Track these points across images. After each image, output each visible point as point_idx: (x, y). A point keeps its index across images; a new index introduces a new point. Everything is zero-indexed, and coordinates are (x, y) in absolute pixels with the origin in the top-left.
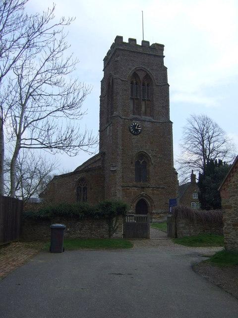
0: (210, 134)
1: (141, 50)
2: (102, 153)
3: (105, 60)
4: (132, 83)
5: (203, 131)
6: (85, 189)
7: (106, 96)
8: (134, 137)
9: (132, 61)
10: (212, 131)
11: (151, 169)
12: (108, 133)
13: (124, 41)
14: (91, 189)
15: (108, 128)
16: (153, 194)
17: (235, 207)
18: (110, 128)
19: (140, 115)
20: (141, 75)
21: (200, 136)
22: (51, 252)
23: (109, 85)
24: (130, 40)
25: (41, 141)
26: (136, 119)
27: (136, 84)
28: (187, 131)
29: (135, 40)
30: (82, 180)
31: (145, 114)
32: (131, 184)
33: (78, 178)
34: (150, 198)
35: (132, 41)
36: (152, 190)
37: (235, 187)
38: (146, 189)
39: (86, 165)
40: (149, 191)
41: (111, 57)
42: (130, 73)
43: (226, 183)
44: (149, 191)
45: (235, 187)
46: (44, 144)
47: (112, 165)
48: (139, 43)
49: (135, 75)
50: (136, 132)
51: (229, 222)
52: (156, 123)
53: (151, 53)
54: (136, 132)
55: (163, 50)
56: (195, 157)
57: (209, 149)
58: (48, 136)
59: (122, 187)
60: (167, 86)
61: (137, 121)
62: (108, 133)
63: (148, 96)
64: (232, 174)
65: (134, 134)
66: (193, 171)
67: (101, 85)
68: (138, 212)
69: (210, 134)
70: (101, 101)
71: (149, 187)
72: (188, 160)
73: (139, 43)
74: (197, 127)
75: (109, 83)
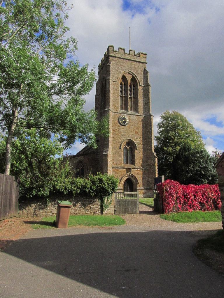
7: (100, 95)
8: (123, 127)
13: (221, 228)
20: (129, 78)
23: (102, 86)
27: (124, 85)
30: (80, 162)
32: (120, 165)
39: (84, 151)
50: (124, 124)
53: (136, 60)
59: (113, 168)
60: (112, 294)
68: (125, 189)
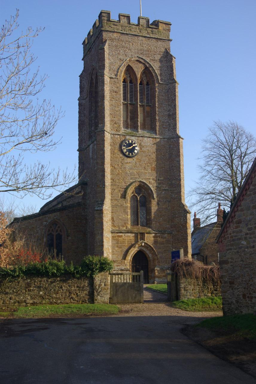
0: (243, 150)
2: (82, 184)
5: (232, 146)
8: (129, 160)
10: (246, 146)
12: (91, 154)
15: (91, 146)
17: (231, 262)
18: (93, 147)
20: (139, 70)
21: (228, 153)
28: (208, 146)
30: (54, 223)
33: (49, 221)
37: (232, 239)
39: (59, 200)
41: (94, 42)
43: (223, 235)
45: (232, 239)
46: (11, 186)
47: (97, 202)
49: (129, 70)
51: (226, 279)
56: (221, 186)
57: (242, 173)
58: (14, 174)
62: (91, 154)
63: (147, 99)
64: (228, 225)
65: (128, 157)
66: (219, 205)
69: (243, 150)
72: (210, 188)
74: (224, 140)
75: (92, 79)
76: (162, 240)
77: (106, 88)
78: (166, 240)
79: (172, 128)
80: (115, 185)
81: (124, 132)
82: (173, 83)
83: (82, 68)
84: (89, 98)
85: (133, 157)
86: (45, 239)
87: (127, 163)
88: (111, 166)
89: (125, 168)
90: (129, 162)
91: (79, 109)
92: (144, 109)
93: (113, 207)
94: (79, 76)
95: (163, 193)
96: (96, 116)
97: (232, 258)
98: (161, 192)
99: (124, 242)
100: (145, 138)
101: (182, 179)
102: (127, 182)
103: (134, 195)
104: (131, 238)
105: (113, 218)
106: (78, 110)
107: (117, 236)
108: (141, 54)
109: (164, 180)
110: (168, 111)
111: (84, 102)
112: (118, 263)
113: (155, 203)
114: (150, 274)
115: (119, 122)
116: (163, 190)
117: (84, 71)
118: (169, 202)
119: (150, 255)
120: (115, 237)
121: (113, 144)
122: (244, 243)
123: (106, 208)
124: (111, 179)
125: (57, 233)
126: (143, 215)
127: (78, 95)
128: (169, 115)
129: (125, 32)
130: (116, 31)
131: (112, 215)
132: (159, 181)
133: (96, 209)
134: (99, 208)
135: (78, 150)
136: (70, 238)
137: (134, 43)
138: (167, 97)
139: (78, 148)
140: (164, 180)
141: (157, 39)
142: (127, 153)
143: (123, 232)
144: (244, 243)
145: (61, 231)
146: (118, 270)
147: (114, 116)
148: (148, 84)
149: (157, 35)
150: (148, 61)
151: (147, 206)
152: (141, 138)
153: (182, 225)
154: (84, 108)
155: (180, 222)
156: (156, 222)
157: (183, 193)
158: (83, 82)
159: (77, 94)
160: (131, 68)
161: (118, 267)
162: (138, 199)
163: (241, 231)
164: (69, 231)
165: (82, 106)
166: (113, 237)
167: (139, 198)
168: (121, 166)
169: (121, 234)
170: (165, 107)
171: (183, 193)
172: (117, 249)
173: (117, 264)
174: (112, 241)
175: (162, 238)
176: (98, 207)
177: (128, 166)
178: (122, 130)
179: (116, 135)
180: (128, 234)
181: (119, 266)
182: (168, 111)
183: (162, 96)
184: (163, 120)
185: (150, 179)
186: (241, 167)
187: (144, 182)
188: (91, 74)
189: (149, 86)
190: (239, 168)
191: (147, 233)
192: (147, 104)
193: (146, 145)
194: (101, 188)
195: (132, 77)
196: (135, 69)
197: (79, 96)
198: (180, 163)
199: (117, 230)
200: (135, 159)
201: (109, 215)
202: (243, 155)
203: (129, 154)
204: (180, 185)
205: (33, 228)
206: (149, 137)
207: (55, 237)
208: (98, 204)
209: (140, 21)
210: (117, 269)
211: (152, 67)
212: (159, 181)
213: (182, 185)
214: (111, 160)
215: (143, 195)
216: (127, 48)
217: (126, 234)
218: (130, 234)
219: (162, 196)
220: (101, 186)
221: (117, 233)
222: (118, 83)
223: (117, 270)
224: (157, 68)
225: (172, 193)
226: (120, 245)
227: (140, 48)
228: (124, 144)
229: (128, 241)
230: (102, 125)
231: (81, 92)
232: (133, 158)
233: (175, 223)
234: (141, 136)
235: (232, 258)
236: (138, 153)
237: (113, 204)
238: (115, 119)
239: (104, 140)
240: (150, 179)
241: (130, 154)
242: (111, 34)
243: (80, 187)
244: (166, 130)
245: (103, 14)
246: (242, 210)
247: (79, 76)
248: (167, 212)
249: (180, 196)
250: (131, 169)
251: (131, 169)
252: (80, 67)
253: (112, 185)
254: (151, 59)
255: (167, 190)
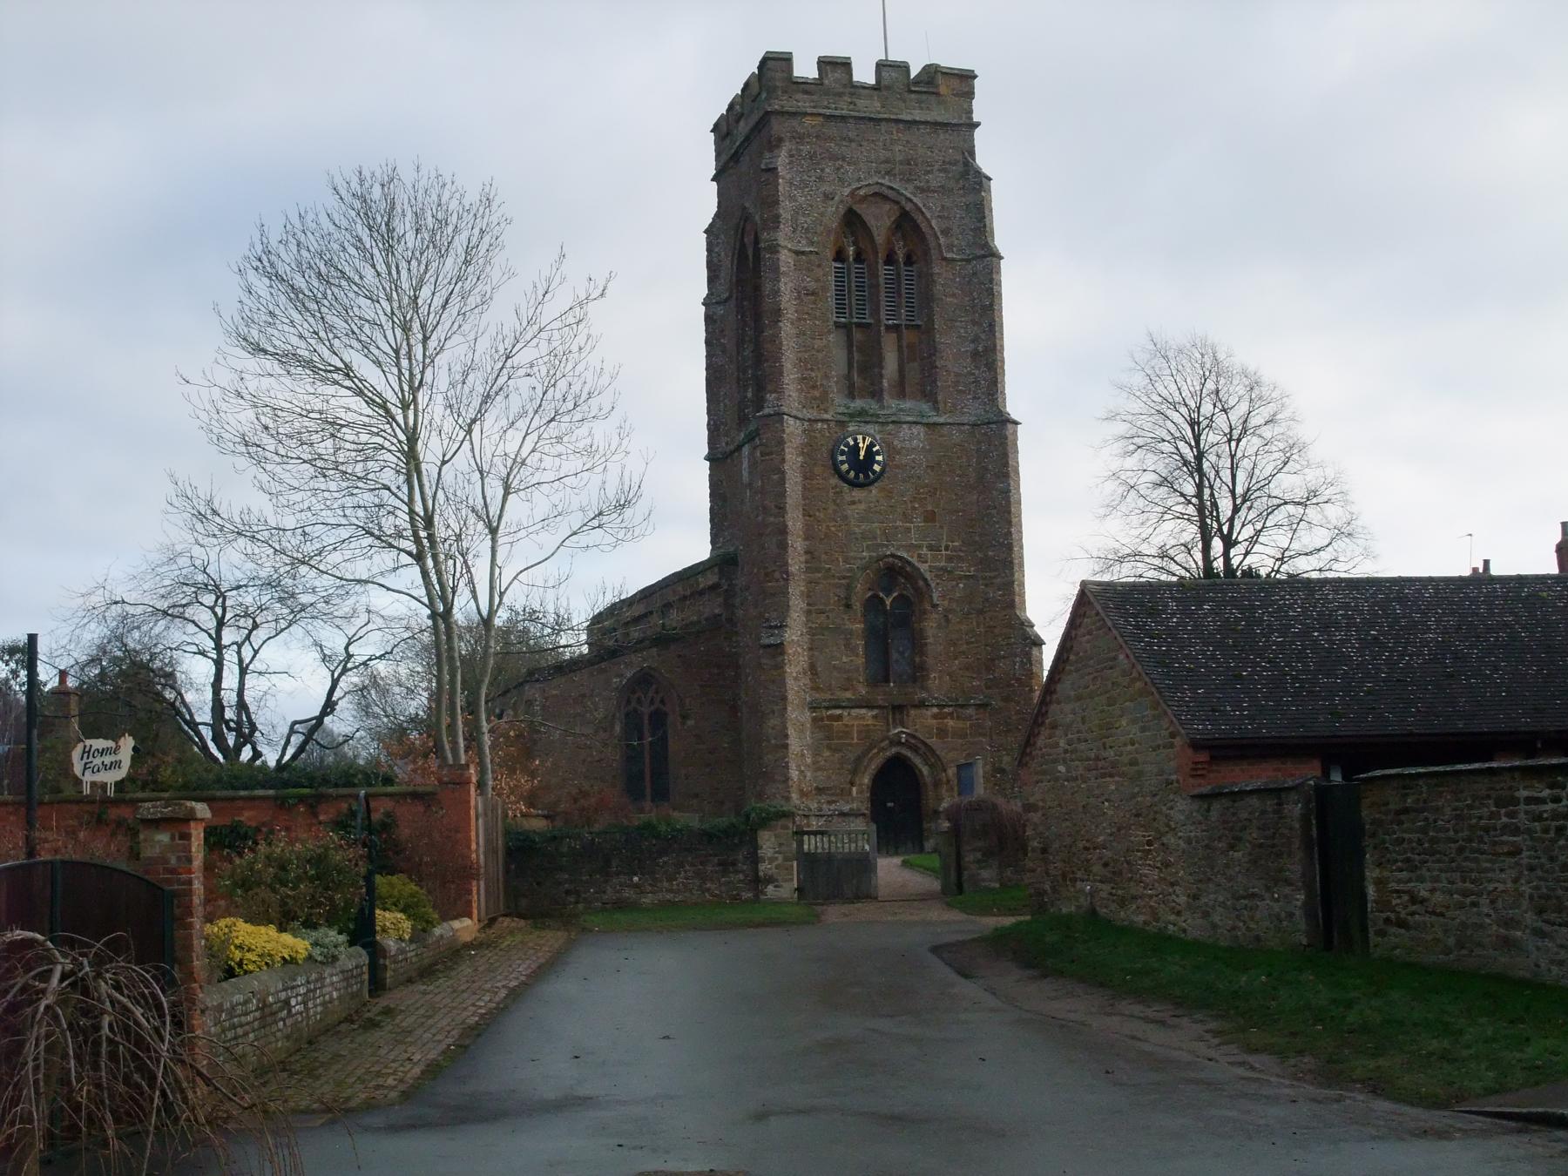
1: (871, 106)
2: (722, 562)
3: (722, 130)
4: (840, 256)
6: (658, 719)
8: (858, 494)
9: (833, 158)
11: (931, 627)
12: (745, 474)
14: (685, 717)
15: (746, 450)
16: (942, 733)
18: (751, 454)
19: (877, 394)
20: (880, 221)
22: (509, 853)
23: (741, 255)
24: (825, 64)
25: (462, 434)
26: (861, 416)
29: (845, 65)
30: (644, 680)
31: (901, 391)
32: (848, 695)
34: (928, 753)
35: (834, 67)
36: (935, 716)
38: (913, 712)
40: (923, 722)
42: (832, 215)
43: (1028, 750)
44: (923, 722)
48: (864, 74)
49: (852, 221)
52: (945, 430)
53: (918, 115)
54: (861, 471)
55: (970, 94)
59: (813, 708)
61: (870, 428)
62: (745, 474)
65: (854, 484)
67: (709, 250)
70: (709, 319)
71: (922, 705)
73: (864, 74)
75: (743, 245)
76: (960, 724)
77: (786, 284)
78: (971, 726)
79: (983, 393)
80: (818, 570)
81: (841, 410)
82: (984, 256)
83: (712, 207)
84: (737, 299)
85: (872, 483)
86: (618, 728)
87: (853, 503)
88: (804, 515)
89: (845, 518)
90: (857, 499)
91: (707, 331)
92: (899, 339)
93: (812, 632)
94: (705, 232)
95: (961, 585)
96: (759, 358)
97: (1043, 800)
98: (954, 583)
99: (847, 734)
100: (904, 426)
101: (1015, 544)
102: (855, 558)
103: (875, 596)
104: (869, 722)
105: (812, 667)
106: (703, 335)
107: (827, 716)
108: (888, 173)
109: (963, 549)
110: (973, 341)
111: (720, 310)
112: (833, 795)
113: (936, 616)
114: (926, 826)
115: (825, 382)
116: (960, 578)
117: (717, 215)
118: (981, 612)
119: (925, 770)
120: (822, 719)
121: (808, 450)
122: (1062, 768)
123: (793, 637)
124: (806, 553)
125: (652, 708)
126: (902, 653)
127: (703, 291)
128: (975, 355)
129: (837, 113)
130: (809, 110)
131: (811, 657)
132: (949, 553)
133: (766, 641)
134: (772, 641)
135: (707, 458)
136: (690, 723)
137: (865, 143)
138: (967, 299)
139: (706, 451)
140: (963, 549)
141: (936, 124)
142: (852, 474)
143: (844, 704)
144: (1062, 768)
145: (662, 701)
146: (831, 815)
147: (809, 366)
148: (909, 261)
149: (932, 113)
150: (909, 195)
151: (916, 625)
152: (891, 427)
153: (1018, 680)
154: (723, 331)
155: (1012, 672)
156: (940, 671)
157: (1019, 585)
158: (716, 250)
159: (697, 286)
160: (859, 216)
161: (832, 808)
162: (886, 605)
163: (1057, 745)
164: (687, 701)
165: (715, 321)
166: (814, 720)
167: (888, 602)
168: (835, 512)
169: (838, 712)
170: (962, 331)
171: (1019, 585)
172: (827, 754)
173: (829, 799)
174: (812, 733)
175: (958, 718)
176: (768, 637)
177: (852, 511)
178: (839, 403)
179: (817, 421)
180: (857, 710)
181: (834, 802)
182: (973, 341)
183: (954, 295)
184: (956, 370)
185: (920, 547)
186: (1232, 472)
187: (903, 558)
188: (740, 231)
189: (915, 266)
190: (1226, 475)
191: (915, 706)
192: (908, 323)
193: (908, 446)
194: (777, 581)
195: (861, 245)
196: (872, 222)
197: (705, 292)
198: (1009, 497)
199: (825, 700)
200: (874, 490)
201: (801, 658)
202: (1236, 434)
203: (857, 476)
204: (1011, 562)
205: (584, 696)
206: (916, 423)
207: (646, 718)
208: (771, 627)
209: (883, 74)
210: (829, 813)
211: (923, 213)
212: (949, 553)
213: (1016, 561)
214: (804, 498)
215: (901, 596)
216: (844, 159)
217: (855, 712)
218: (863, 711)
219: (958, 595)
220: (777, 575)
221: (828, 708)
222: (819, 266)
223: (828, 816)
224: (937, 214)
225: (986, 585)
226: (836, 741)
227: (883, 154)
228: (842, 447)
229: (859, 732)
230: (773, 395)
231: (711, 280)
232: (871, 488)
233: (996, 675)
234: (890, 420)
235: (1043, 800)
236: (883, 471)
237: (814, 626)
238: (813, 374)
239: (781, 442)
240: (920, 547)
241: (861, 475)
242: (794, 123)
243: (716, 570)
244: (968, 400)
245: (769, 62)
246: (1059, 703)
247: (705, 232)
248: (972, 643)
249: (1012, 593)
250: (862, 520)
251: (862, 520)
252: (705, 202)
253: (808, 570)
254: (917, 188)
255: (971, 576)
